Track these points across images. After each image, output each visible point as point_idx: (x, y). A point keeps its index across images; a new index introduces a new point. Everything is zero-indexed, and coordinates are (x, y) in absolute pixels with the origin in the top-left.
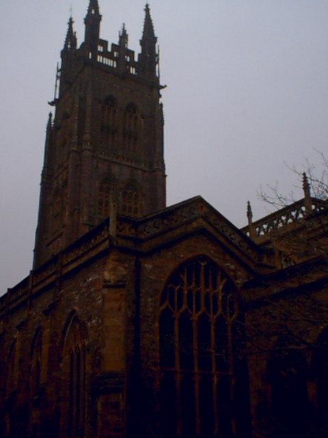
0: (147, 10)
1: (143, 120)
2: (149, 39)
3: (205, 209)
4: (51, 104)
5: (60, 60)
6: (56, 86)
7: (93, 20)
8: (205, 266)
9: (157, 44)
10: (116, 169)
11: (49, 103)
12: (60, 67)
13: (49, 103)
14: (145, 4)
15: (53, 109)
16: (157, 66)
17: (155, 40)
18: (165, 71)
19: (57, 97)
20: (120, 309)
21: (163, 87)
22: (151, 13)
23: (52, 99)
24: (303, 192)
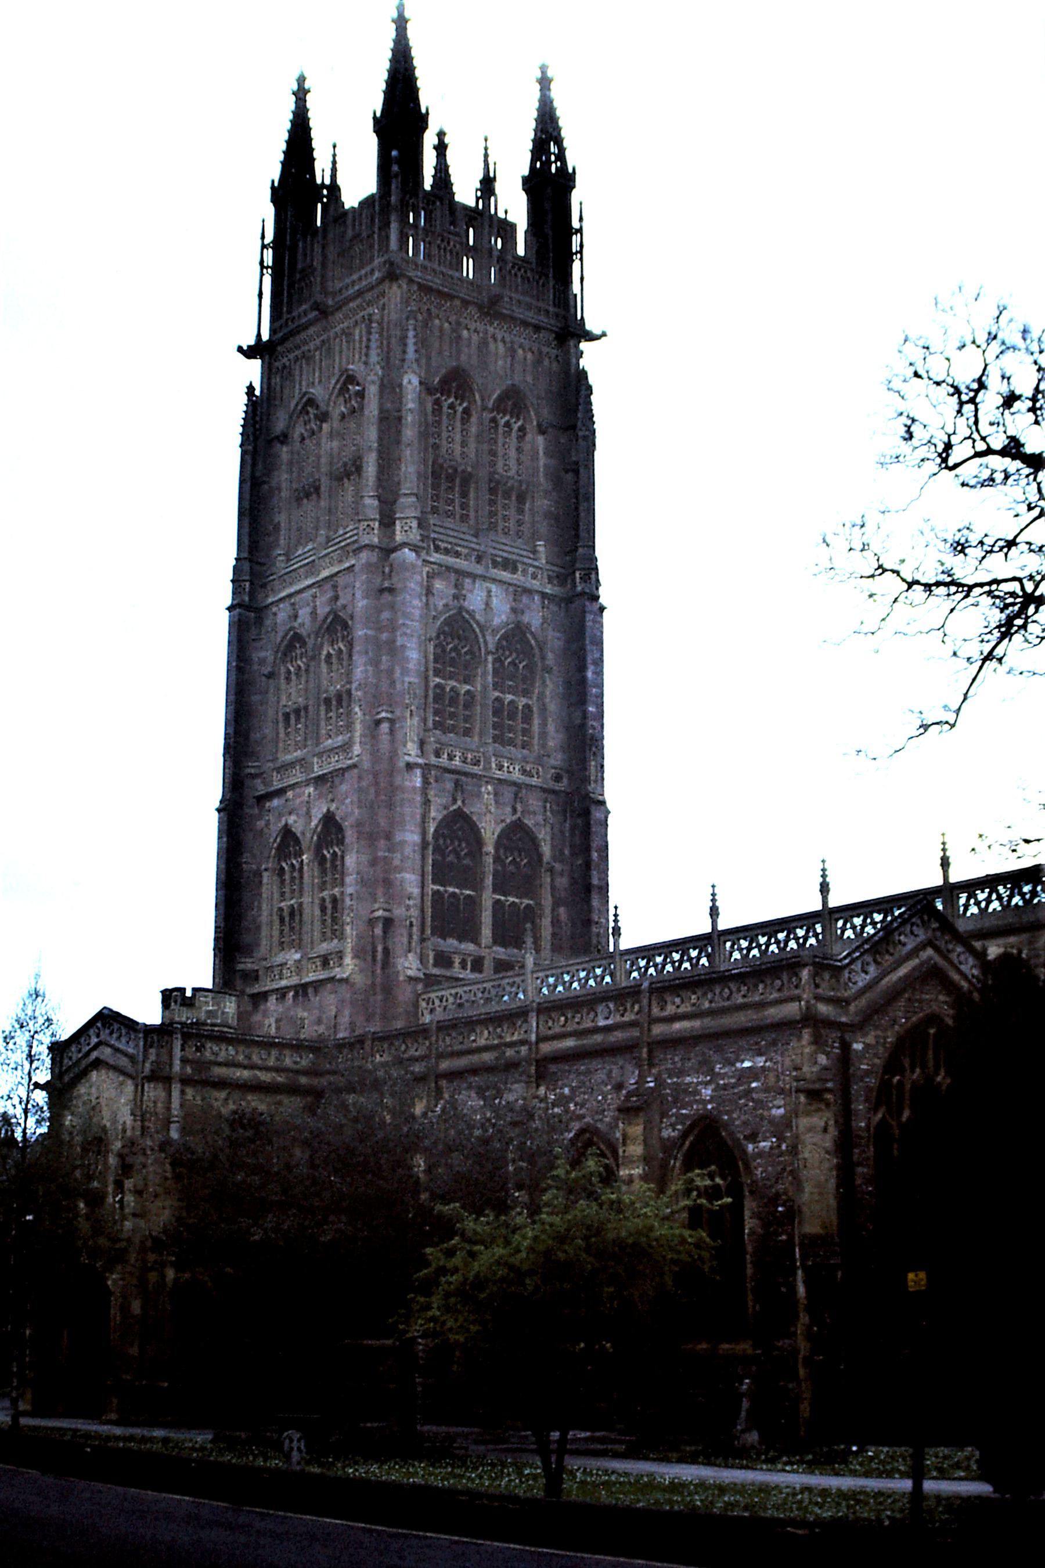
0: (301, 95)
1: (540, 439)
2: (550, 185)
3: (603, 876)
4: (249, 353)
5: (269, 212)
6: (260, 295)
7: (401, 118)
8: (934, 1034)
9: (576, 197)
10: (475, 599)
11: (240, 349)
12: (269, 237)
13: (240, 349)
14: (297, 76)
15: (255, 365)
16: (576, 266)
17: (566, 181)
18: (603, 284)
19: (265, 336)
20: (825, 1130)
21: (591, 337)
22: (311, 101)
23: (249, 340)
24: (709, 921)
